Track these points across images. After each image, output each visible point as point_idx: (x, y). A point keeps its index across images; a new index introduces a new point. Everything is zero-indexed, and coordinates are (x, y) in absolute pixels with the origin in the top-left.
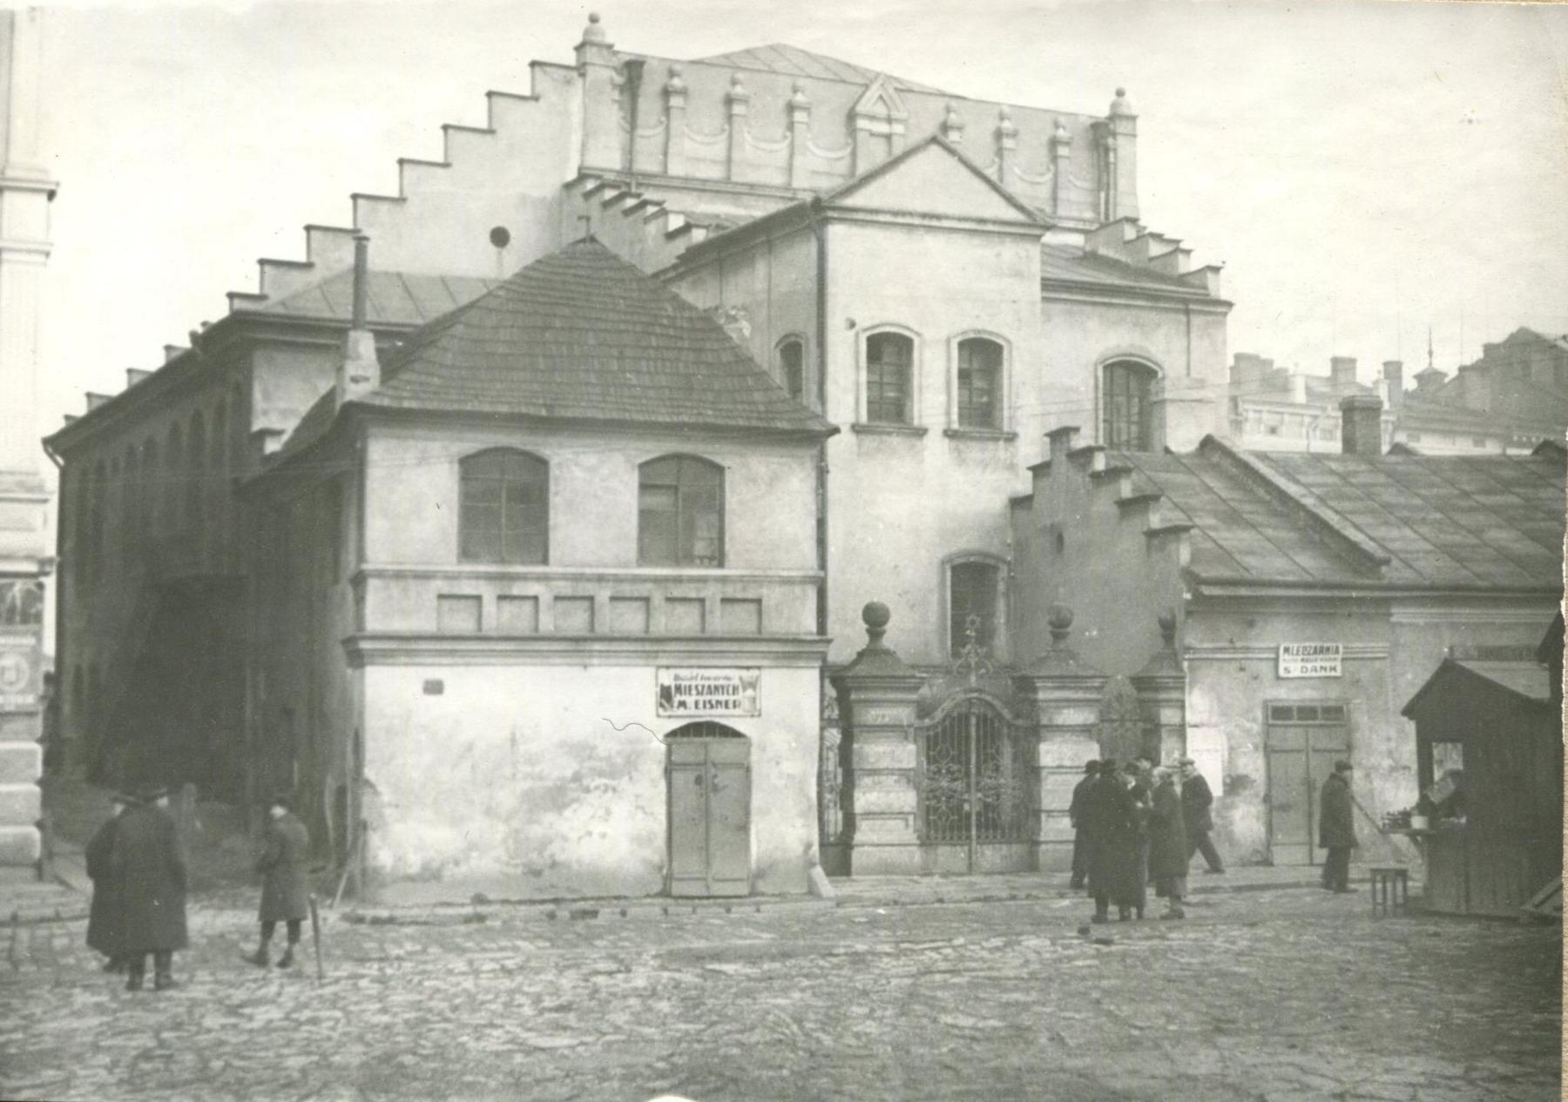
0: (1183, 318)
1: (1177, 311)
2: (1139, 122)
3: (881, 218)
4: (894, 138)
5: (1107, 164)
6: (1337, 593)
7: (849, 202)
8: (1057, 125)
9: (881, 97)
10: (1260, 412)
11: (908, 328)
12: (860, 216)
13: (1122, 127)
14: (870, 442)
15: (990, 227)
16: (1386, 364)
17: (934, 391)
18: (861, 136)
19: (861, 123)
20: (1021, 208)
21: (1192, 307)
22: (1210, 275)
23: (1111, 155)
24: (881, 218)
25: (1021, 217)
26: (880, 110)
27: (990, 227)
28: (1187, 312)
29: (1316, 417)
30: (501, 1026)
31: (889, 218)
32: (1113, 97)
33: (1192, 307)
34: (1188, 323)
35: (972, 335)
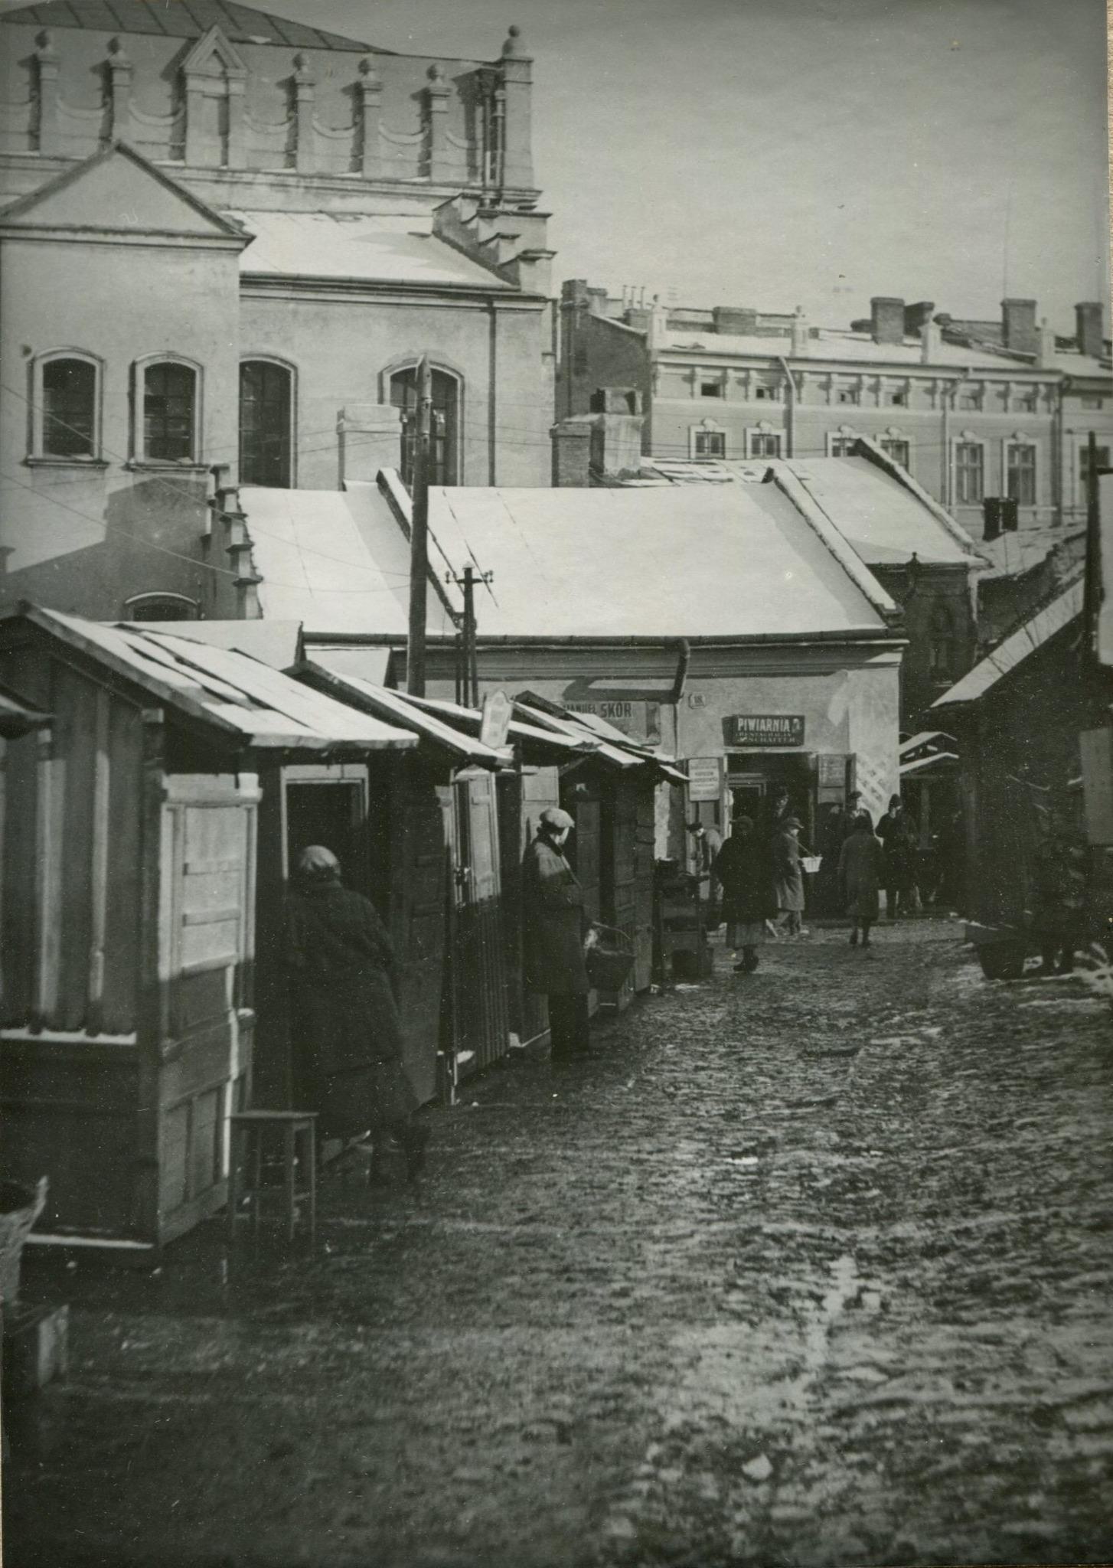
0: (487, 316)
1: (483, 310)
2: (535, 69)
3: (59, 235)
4: (232, 99)
5: (494, 120)
6: (612, 648)
7: (25, 219)
8: (432, 74)
9: (215, 52)
10: (877, 376)
11: (92, 356)
12: (37, 234)
13: (513, 73)
14: (48, 476)
15: (181, 241)
16: (1079, 308)
17: (118, 425)
18: (192, 99)
19: (192, 84)
20: (217, 220)
21: (496, 304)
22: (522, 266)
23: (500, 106)
24: (59, 235)
25: (215, 230)
26: (215, 67)
27: (181, 241)
28: (492, 311)
29: (953, 381)
30: (380, 1336)
31: (69, 236)
32: (507, 36)
33: (496, 304)
34: (493, 323)
35: (161, 360)
